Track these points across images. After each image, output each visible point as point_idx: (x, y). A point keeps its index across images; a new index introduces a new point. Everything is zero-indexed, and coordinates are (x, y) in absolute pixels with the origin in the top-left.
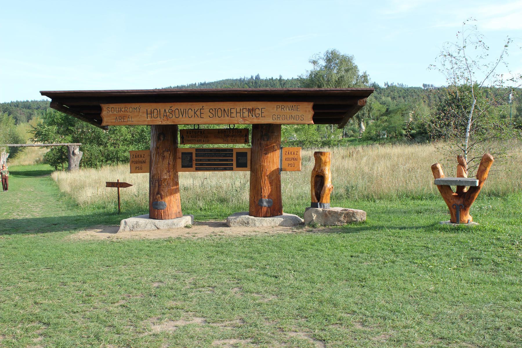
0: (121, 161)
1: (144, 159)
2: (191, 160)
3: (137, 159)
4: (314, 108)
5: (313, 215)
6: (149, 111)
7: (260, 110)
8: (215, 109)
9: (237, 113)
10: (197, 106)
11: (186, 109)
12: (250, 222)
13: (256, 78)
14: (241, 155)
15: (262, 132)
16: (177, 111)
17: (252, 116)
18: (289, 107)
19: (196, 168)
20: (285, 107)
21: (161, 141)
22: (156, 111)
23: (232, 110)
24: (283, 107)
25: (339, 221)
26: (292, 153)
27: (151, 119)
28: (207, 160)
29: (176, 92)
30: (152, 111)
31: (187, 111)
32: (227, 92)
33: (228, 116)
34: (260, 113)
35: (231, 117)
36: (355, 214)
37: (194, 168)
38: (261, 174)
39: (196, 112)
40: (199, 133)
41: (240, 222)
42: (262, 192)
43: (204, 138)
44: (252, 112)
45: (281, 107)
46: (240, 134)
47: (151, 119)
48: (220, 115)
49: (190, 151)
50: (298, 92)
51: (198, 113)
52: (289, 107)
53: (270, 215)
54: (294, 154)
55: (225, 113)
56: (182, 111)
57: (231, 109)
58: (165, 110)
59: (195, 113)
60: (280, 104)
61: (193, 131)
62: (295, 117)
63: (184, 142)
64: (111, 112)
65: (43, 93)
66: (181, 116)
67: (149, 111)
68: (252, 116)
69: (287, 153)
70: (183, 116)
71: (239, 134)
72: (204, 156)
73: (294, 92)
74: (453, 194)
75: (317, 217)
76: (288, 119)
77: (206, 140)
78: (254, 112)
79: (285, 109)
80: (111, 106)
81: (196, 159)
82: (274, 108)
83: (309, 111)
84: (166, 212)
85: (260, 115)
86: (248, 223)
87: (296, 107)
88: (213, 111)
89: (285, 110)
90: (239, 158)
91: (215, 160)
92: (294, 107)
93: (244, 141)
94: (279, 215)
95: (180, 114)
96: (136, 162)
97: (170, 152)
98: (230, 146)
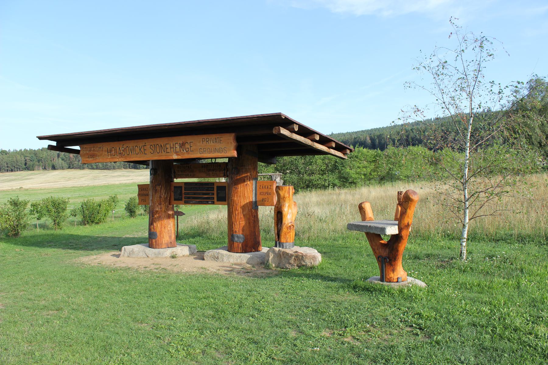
0: (319, 187)
2: (181, 194)
5: (270, 255)
6: (109, 149)
7: (189, 144)
8: (154, 145)
10: (141, 143)
12: (219, 257)
13: (488, 111)
14: (221, 188)
16: (127, 148)
18: (213, 139)
19: (185, 201)
23: (167, 145)
24: (208, 140)
25: (290, 264)
26: (266, 187)
27: (111, 157)
28: (193, 194)
31: (134, 148)
32: (151, 129)
33: (164, 151)
34: (189, 147)
36: (304, 257)
37: (183, 202)
38: (232, 208)
40: (187, 168)
41: (212, 256)
42: (233, 227)
44: (182, 147)
47: (111, 157)
49: (180, 185)
50: (209, 123)
51: (142, 150)
52: (213, 139)
53: (243, 251)
54: (268, 188)
55: (162, 149)
56: (131, 148)
57: (167, 145)
58: (119, 148)
59: (140, 150)
60: (205, 137)
61: (211, 165)
62: (219, 150)
65: (41, 138)
66: (131, 153)
67: (109, 149)
68: (183, 151)
69: (261, 187)
70: (132, 152)
72: (191, 190)
73: (204, 123)
74: (380, 241)
75: (273, 257)
76: (213, 152)
78: (184, 147)
79: (209, 142)
81: (185, 193)
82: (200, 141)
84: (157, 242)
85: (190, 149)
86: (218, 258)
87: (219, 139)
90: (219, 192)
91: (199, 194)
93: (223, 175)
94: (254, 252)
95: (130, 151)
97: (162, 186)
98: (211, 180)
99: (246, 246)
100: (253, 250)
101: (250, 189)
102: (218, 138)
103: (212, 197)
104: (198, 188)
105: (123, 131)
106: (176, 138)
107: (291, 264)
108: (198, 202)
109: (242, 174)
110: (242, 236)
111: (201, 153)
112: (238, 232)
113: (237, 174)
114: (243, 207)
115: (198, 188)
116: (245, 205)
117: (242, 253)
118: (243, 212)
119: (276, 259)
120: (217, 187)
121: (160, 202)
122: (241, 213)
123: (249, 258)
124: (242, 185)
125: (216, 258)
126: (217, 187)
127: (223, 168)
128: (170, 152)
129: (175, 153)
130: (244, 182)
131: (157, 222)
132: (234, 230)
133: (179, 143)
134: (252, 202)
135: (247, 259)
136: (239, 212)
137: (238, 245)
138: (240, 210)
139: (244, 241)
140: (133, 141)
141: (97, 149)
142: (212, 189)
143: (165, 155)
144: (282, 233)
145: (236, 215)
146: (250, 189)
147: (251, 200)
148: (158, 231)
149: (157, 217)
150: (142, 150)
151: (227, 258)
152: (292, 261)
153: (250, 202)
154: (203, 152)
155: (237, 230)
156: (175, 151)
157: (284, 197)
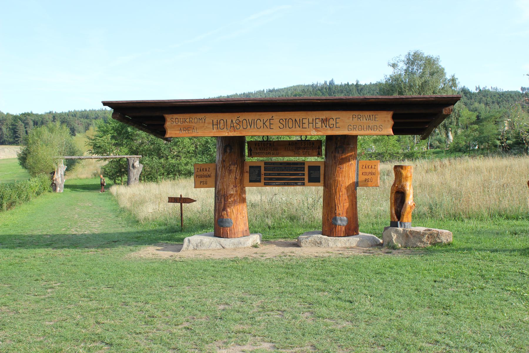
1: (209, 173)
2: (259, 175)
3: (202, 173)
4: (394, 117)
5: (393, 236)
6: (215, 121)
7: (335, 120)
9: (309, 123)
10: (266, 116)
11: (254, 120)
13: (330, 83)
14: (314, 169)
15: (337, 144)
16: (244, 121)
17: (326, 127)
20: (362, 116)
21: (228, 154)
22: (222, 122)
23: (303, 120)
24: (359, 116)
26: (370, 167)
29: (244, 102)
30: (219, 121)
31: (255, 121)
33: (300, 127)
34: (335, 123)
35: (302, 128)
36: (440, 234)
39: (265, 122)
40: (268, 145)
41: (312, 242)
43: (274, 150)
44: (325, 123)
45: (357, 116)
46: (312, 146)
47: (218, 130)
48: (291, 126)
49: (258, 165)
50: (377, 100)
51: (267, 124)
53: (345, 235)
54: (371, 168)
56: (250, 122)
58: (232, 121)
60: (356, 113)
61: (262, 143)
62: (373, 128)
63: (252, 154)
64: (174, 123)
65: (105, 104)
66: (249, 127)
68: (326, 127)
69: (364, 167)
70: (251, 126)
71: (311, 146)
72: (274, 170)
75: (397, 238)
77: (276, 153)
78: (328, 123)
79: (361, 119)
80: (175, 116)
82: (350, 117)
83: (388, 121)
84: (233, 229)
86: (321, 243)
87: (374, 116)
88: (283, 121)
89: (362, 120)
90: (311, 172)
91: (285, 174)
92: (371, 116)
93: (317, 153)
94: (355, 235)
95: (248, 125)
96: (201, 176)
97: (237, 166)
98: (301, 159)
99: (349, 229)
100: (355, 233)
101: (353, 169)
102: (373, 115)
103: (266, 180)
104: (284, 168)
105: (255, 102)
106: (310, 113)
107: (424, 242)
108: (283, 184)
109: (348, 153)
110: (345, 218)
111: (350, 130)
112: (341, 214)
113: (343, 153)
114: (348, 188)
115: (284, 168)
116: (349, 185)
117: (345, 236)
118: (347, 193)
119: (401, 239)
120: (309, 166)
121: (235, 184)
122: (345, 194)
123: (359, 241)
124: (347, 164)
125: (318, 244)
126: (309, 167)
127: (318, 147)
128: (320, 127)
129: (314, 129)
130: (349, 161)
131: (232, 207)
132: (337, 213)
133: (321, 118)
134: (355, 182)
135: (356, 243)
136: (344, 193)
137: (341, 228)
138: (344, 191)
139: (347, 224)
140: (254, 113)
141: (196, 120)
142: (302, 169)
143: (300, 131)
144: (406, 213)
145: (340, 196)
146: (353, 169)
147: (354, 181)
148: (233, 217)
149: (232, 201)
150: (267, 124)
151: (333, 243)
152: (425, 239)
153: (353, 183)
154: (352, 129)
155: (341, 212)
156: (314, 127)
157: (406, 177)
